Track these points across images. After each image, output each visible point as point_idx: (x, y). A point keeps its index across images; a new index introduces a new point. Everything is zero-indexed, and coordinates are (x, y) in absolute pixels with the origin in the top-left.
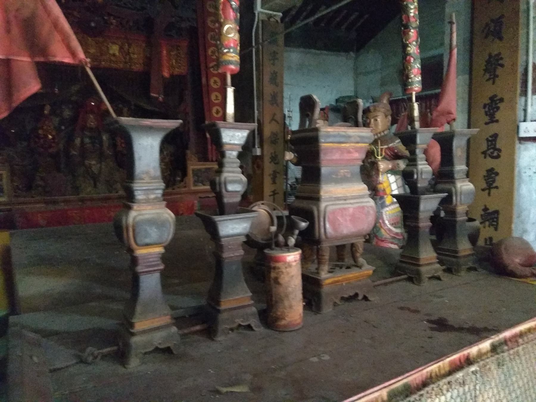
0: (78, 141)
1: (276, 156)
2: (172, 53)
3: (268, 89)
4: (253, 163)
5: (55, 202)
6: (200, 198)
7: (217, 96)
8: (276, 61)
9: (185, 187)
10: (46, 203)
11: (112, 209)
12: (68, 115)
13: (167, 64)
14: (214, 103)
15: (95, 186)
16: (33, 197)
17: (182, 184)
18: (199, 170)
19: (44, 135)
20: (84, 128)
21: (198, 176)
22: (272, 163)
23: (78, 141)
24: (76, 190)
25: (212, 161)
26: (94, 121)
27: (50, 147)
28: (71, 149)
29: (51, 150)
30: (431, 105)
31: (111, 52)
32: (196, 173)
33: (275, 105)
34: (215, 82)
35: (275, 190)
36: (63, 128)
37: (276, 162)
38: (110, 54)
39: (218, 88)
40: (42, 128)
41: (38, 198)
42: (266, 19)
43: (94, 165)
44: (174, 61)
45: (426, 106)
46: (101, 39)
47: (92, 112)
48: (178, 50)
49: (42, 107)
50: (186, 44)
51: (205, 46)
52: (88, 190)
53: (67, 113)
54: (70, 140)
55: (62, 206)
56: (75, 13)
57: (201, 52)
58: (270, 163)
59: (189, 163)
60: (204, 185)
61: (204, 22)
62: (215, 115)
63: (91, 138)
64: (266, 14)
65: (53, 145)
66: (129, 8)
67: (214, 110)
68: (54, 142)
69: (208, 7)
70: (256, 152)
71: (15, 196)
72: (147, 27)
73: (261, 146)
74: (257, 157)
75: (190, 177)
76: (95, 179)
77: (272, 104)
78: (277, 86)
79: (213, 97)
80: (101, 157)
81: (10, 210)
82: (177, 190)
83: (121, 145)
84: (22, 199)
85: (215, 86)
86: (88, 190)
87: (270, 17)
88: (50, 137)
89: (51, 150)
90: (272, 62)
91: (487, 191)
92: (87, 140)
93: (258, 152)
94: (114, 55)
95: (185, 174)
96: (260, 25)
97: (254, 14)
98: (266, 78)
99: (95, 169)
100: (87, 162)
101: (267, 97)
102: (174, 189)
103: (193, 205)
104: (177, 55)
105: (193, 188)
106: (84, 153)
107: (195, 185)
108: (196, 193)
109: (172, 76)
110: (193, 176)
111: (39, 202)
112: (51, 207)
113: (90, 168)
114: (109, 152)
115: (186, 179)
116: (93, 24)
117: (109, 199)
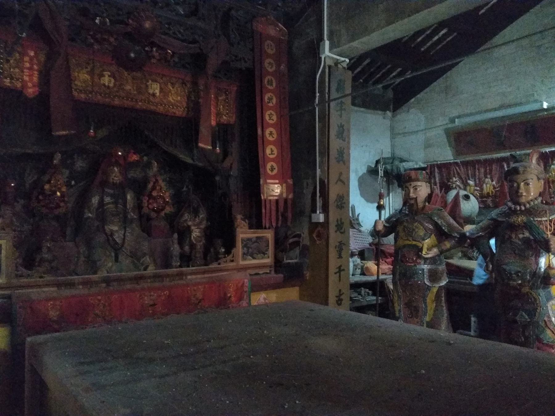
0: (95, 200)
1: (342, 223)
2: (220, 98)
3: (335, 144)
4: (311, 233)
5: (71, 285)
6: (250, 275)
7: (272, 151)
8: (343, 112)
9: (232, 261)
10: (59, 285)
11: (147, 293)
12: (80, 167)
13: (214, 111)
14: (269, 158)
15: (117, 260)
16: (41, 277)
17: (229, 258)
18: (249, 239)
19: (51, 191)
20: (104, 184)
21: (248, 248)
22: (338, 232)
23: (95, 200)
24: (93, 267)
25: (265, 228)
26: (118, 174)
27: (58, 206)
28: (86, 211)
29: (57, 212)
30: (491, 170)
31: (151, 91)
32: (246, 243)
33: (341, 162)
34: (271, 134)
35: (340, 266)
36: (73, 183)
37: (342, 231)
38: (149, 94)
39: (274, 141)
40: (49, 182)
41: (48, 278)
42: (333, 65)
43: (117, 231)
44: (221, 106)
45: (485, 171)
46: (139, 75)
47: (117, 164)
48: (226, 95)
49: (52, 157)
50: (235, 88)
51: (261, 92)
52: (108, 267)
53: (80, 164)
54: (83, 200)
55: (81, 291)
56: (112, 40)
57: (258, 99)
58: (336, 232)
59: (238, 230)
60: (254, 258)
61: (261, 63)
62: (269, 172)
63: (112, 196)
64: (333, 58)
65: (62, 204)
66: (178, 39)
67: (269, 166)
68: (64, 201)
69: (266, 48)
70: (318, 219)
71: (17, 276)
72: (197, 63)
73: (325, 209)
74: (318, 224)
75: (239, 249)
76: (117, 249)
77: (338, 162)
78: (344, 140)
79: (268, 151)
80: (125, 222)
81: (9, 297)
82: (223, 265)
83: (148, 206)
84: (24, 280)
85: (271, 139)
86: (108, 267)
87: (337, 63)
88: (58, 194)
89: (57, 212)
90: (339, 113)
91: (338, 274)
92: (107, 199)
93: (321, 218)
94: (154, 95)
95: (230, 245)
96: (327, 70)
97: (320, 58)
98: (333, 132)
99: (118, 238)
100: (108, 228)
101: (333, 153)
102: (219, 264)
103: (243, 285)
104: (225, 101)
105: (242, 263)
106: (102, 215)
107: (244, 259)
108: (245, 268)
109: (219, 124)
110: (243, 248)
111: (47, 285)
112: (67, 292)
113: (112, 235)
114: (132, 215)
115: (233, 251)
116: (132, 55)
117: (141, 278)
